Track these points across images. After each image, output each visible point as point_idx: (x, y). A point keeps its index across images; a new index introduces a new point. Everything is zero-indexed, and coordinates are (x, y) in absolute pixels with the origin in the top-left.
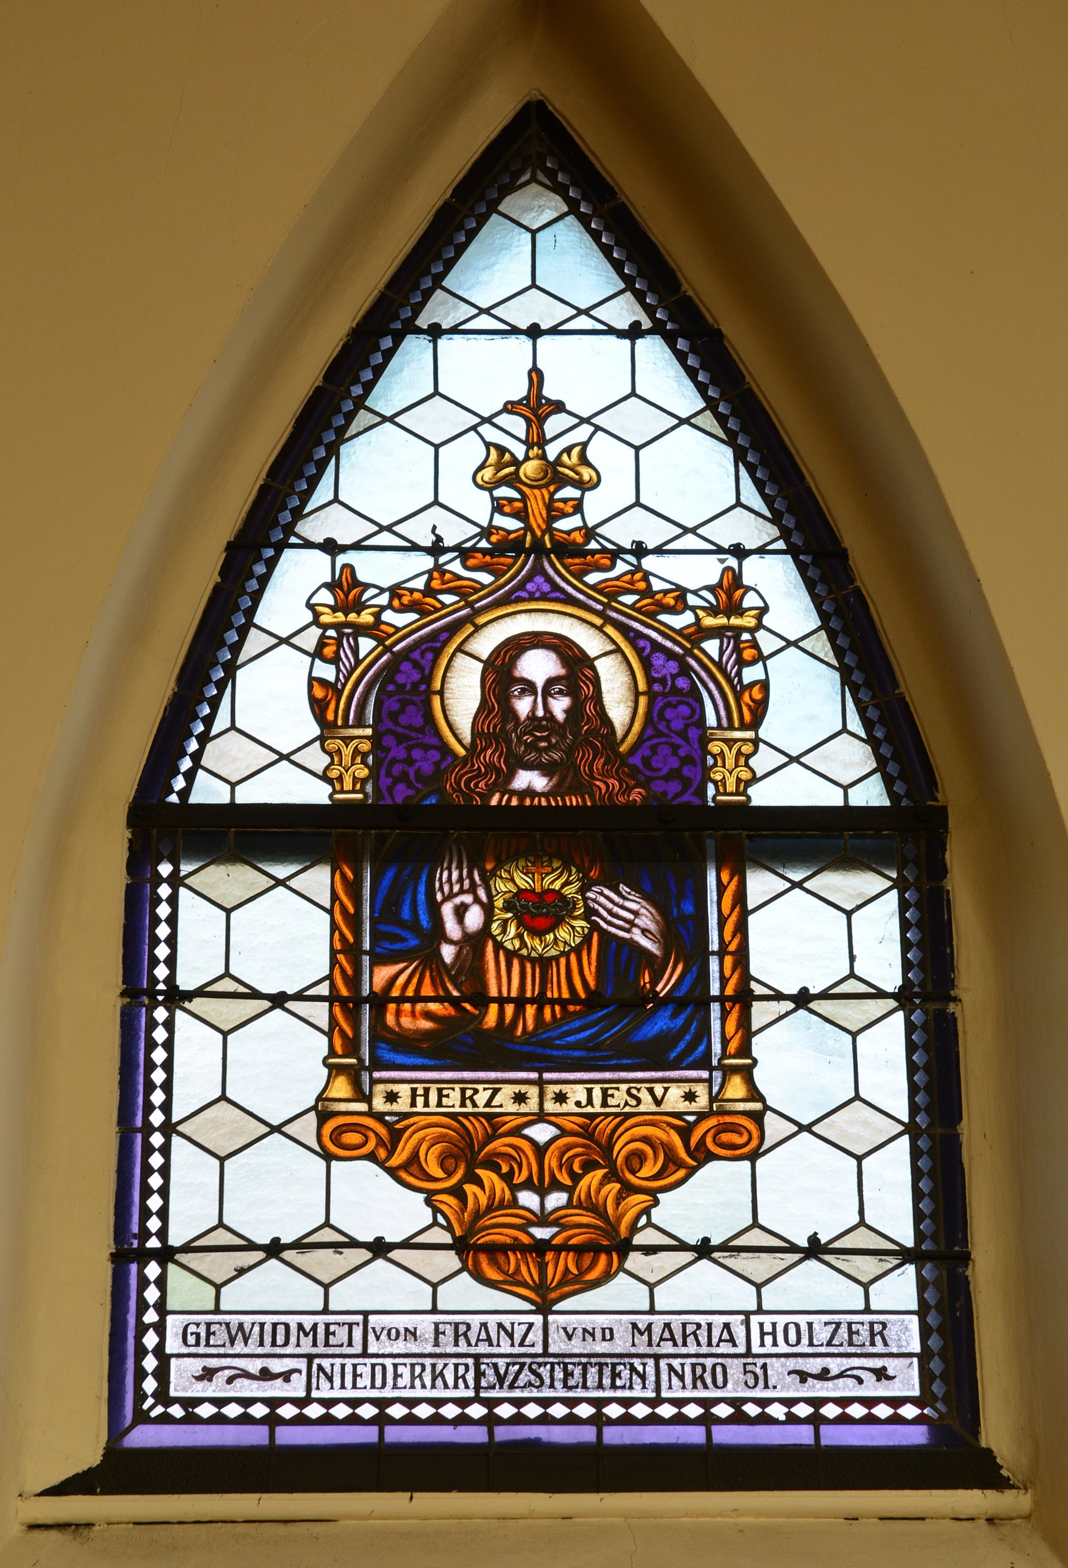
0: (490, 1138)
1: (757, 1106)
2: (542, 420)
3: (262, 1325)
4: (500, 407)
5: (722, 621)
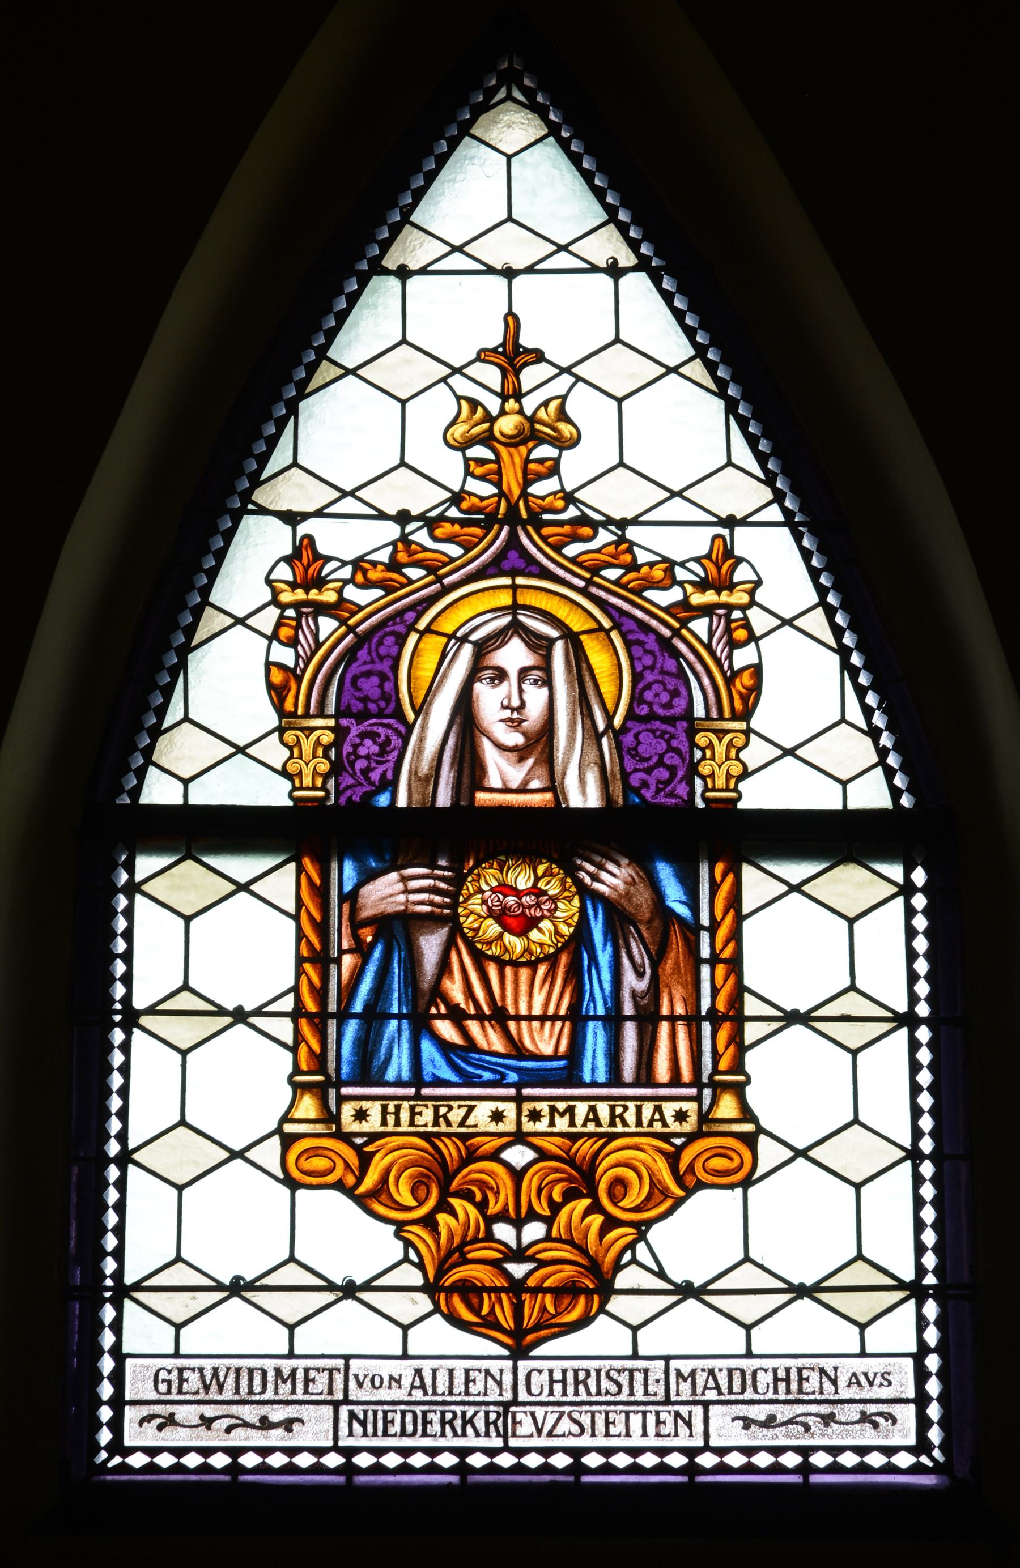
0: (464, 1162)
1: (748, 1127)
2: (517, 372)
3: (238, 1371)
4: (474, 356)
5: (710, 597)
